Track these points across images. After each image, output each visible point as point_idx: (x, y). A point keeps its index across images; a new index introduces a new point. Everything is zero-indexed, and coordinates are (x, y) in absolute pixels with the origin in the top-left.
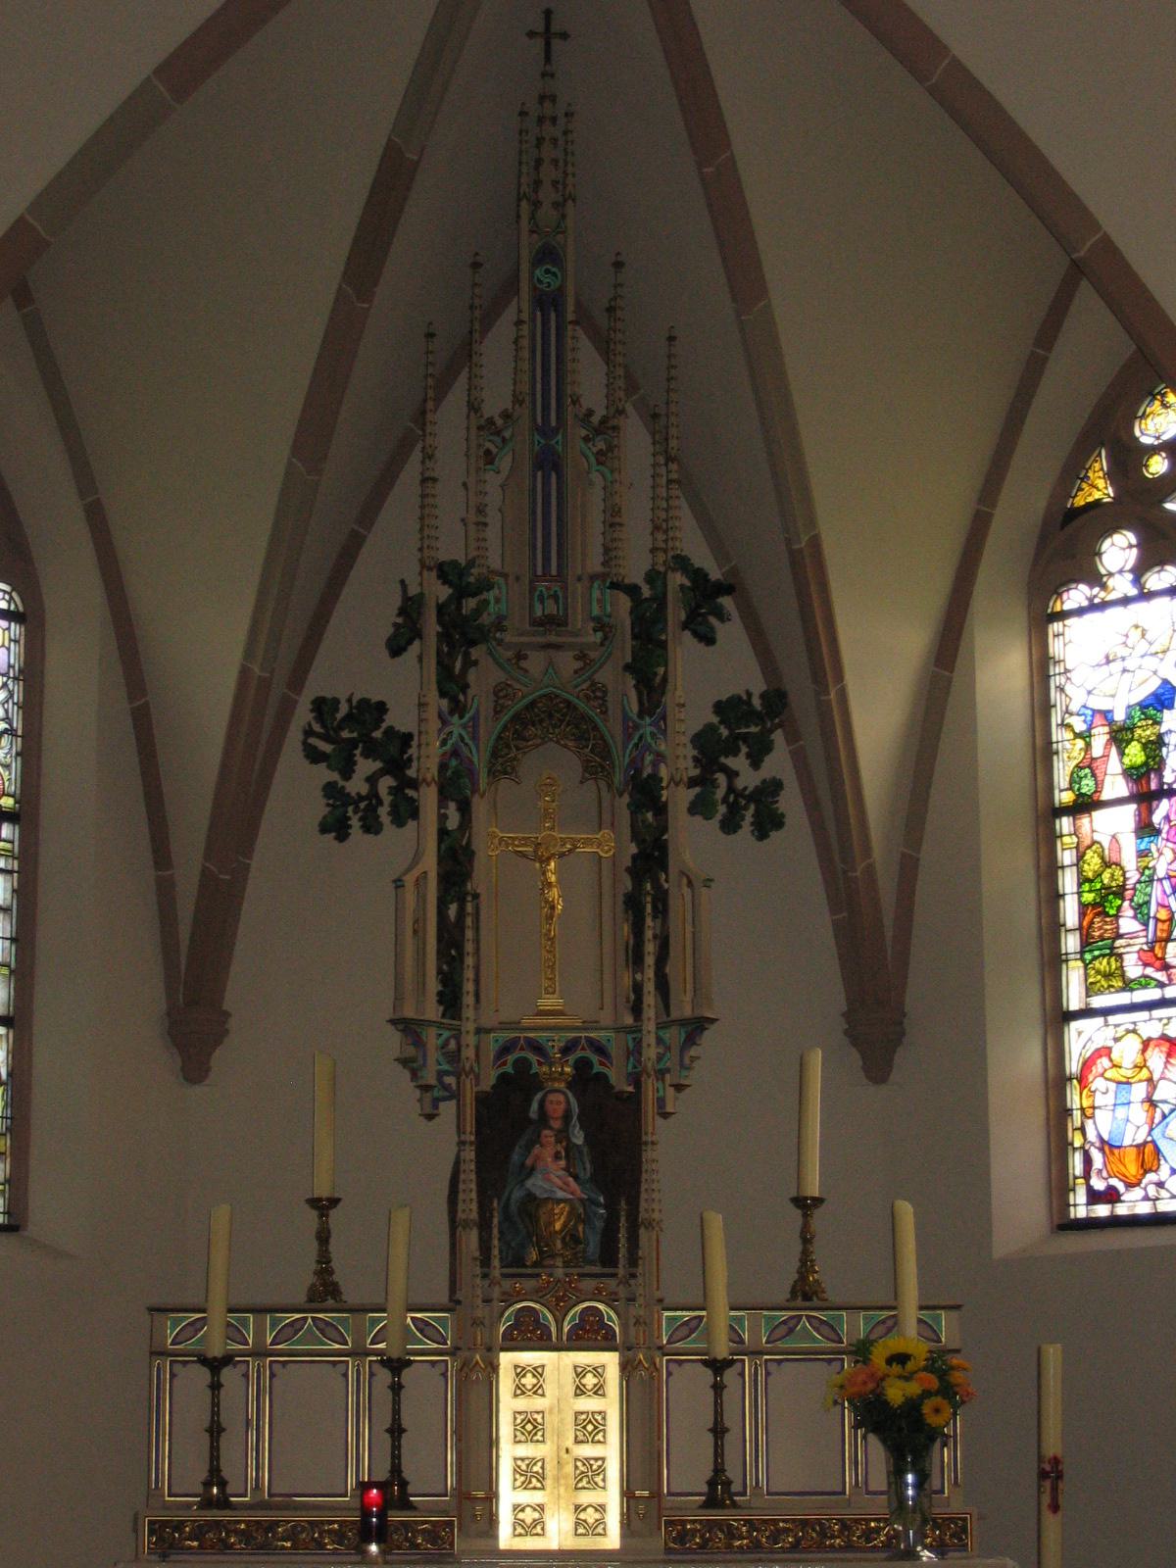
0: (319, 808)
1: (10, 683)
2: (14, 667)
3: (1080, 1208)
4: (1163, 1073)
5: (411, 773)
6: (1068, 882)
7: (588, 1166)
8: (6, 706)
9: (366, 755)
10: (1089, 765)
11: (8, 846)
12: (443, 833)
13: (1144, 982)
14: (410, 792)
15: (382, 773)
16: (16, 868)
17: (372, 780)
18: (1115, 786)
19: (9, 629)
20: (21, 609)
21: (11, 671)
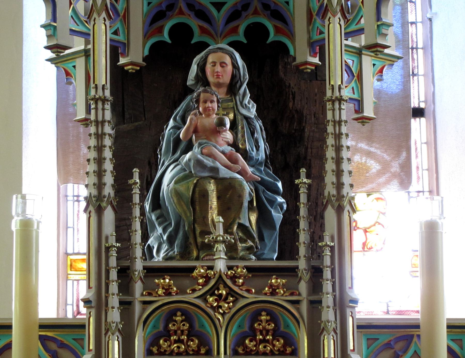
7: (262, 144)
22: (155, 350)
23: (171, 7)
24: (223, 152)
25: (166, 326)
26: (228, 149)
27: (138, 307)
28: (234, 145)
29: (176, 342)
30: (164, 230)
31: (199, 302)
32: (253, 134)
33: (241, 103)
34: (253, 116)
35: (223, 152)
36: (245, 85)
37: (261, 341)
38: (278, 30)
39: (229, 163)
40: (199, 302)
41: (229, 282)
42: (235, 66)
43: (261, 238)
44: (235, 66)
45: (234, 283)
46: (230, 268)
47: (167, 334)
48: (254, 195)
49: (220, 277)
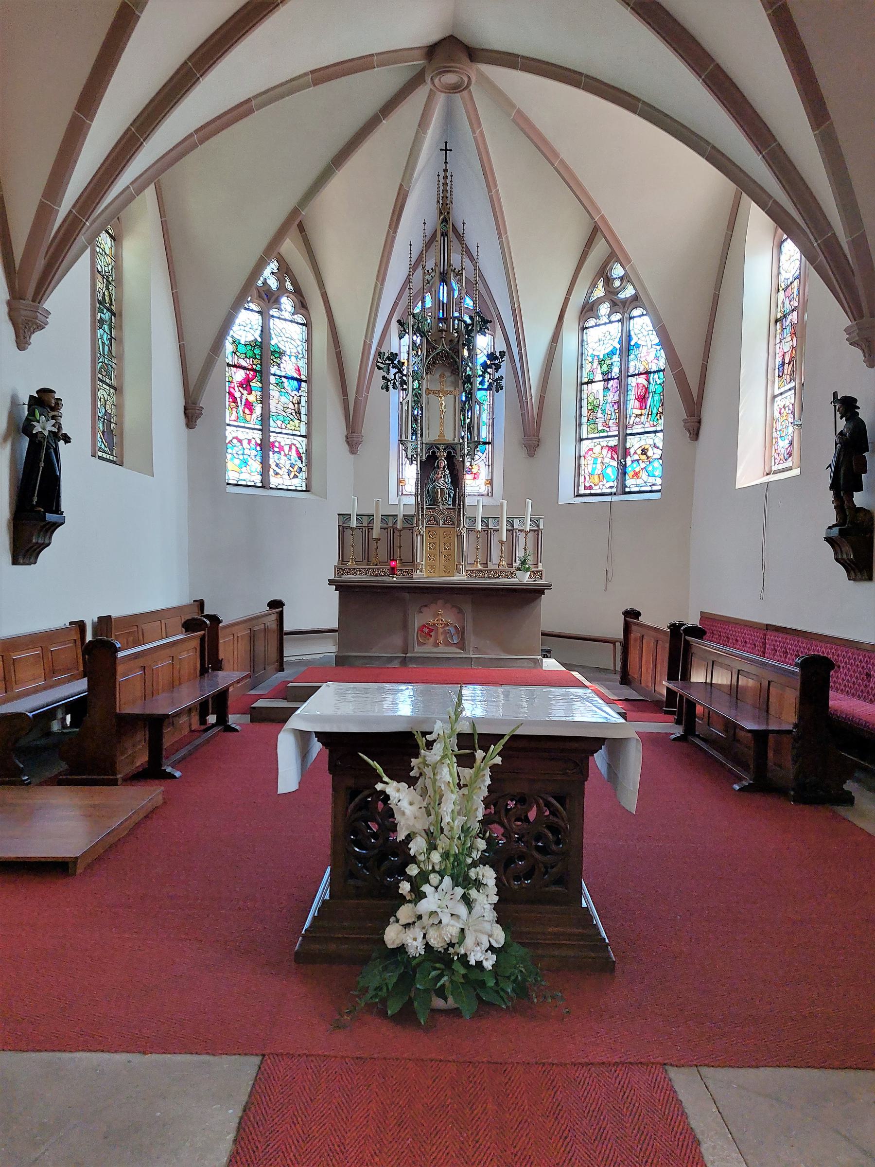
0: (382, 382)
3: (582, 492)
6: (584, 403)
9: (393, 367)
10: (592, 371)
12: (413, 389)
13: (603, 431)
14: (404, 378)
17: (395, 375)
18: (599, 377)
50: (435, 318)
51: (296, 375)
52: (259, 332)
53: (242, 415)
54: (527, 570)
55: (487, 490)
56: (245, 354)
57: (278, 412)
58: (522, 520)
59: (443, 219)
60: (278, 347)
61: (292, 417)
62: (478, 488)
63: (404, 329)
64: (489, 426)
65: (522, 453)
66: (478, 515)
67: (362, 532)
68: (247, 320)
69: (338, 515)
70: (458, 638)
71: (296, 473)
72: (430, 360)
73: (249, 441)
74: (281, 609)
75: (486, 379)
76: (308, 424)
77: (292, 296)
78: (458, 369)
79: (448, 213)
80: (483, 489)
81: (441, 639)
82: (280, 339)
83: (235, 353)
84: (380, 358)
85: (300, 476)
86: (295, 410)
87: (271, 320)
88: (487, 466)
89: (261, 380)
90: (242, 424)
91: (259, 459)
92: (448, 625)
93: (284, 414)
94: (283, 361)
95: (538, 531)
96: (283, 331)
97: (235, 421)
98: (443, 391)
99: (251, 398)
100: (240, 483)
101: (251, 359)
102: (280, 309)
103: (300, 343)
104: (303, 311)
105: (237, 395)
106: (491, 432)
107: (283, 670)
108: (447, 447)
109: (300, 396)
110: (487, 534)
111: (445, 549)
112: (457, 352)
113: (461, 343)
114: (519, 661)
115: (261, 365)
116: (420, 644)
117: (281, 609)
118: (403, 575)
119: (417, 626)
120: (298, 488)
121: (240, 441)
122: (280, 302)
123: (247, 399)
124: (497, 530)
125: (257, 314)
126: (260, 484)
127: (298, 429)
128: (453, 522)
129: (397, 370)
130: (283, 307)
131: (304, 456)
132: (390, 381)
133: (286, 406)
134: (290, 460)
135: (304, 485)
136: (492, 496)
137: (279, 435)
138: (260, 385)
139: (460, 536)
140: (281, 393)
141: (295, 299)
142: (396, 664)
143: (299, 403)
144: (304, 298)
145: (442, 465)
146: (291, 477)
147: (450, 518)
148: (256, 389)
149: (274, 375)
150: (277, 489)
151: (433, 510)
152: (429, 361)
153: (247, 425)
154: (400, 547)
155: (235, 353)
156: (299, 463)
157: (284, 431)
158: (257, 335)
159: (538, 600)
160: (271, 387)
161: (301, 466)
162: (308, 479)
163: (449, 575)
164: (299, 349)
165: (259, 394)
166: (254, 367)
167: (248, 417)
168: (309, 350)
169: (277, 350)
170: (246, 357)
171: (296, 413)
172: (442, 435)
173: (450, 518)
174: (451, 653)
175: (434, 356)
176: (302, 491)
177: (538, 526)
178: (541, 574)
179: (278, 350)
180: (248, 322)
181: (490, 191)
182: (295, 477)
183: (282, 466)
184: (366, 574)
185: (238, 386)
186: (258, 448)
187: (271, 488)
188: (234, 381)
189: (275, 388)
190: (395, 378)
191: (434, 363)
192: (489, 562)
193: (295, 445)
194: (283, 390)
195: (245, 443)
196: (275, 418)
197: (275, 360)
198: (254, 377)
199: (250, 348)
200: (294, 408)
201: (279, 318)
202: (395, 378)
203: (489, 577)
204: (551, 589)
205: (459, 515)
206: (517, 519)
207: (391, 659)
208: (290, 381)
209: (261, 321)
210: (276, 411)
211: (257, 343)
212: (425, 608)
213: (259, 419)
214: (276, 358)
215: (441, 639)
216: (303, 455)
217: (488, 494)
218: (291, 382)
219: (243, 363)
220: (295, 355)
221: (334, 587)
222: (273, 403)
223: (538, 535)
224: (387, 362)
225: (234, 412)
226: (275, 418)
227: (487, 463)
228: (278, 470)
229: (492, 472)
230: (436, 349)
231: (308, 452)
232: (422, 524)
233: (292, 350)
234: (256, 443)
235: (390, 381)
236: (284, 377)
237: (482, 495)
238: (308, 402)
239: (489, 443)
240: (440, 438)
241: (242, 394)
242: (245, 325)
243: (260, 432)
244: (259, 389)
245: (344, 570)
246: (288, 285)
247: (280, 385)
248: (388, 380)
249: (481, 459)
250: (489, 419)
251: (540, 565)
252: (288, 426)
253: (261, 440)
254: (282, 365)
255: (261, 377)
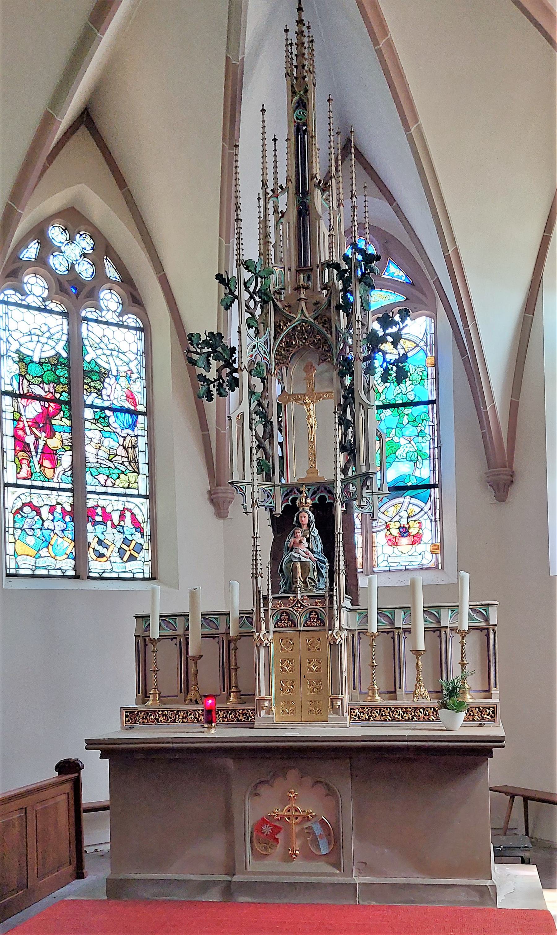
1: (139, 357)
2: (140, 351)
4: (48, 549)
5: (236, 366)
7: (319, 545)
8: (137, 367)
11: (143, 426)
12: (252, 393)
14: (235, 375)
15: (224, 367)
16: (146, 435)
19: (136, 334)
20: (142, 326)
21: (139, 352)
22: (276, 626)
23: (291, 491)
24: (303, 551)
25: (280, 618)
26: (305, 550)
27: (270, 611)
28: (308, 548)
29: (284, 623)
30: (284, 580)
31: (291, 609)
32: (316, 542)
33: (312, 530)
34: (316, 535)
35: (303, 551)
36: (314, 523)
37: (313, 622)
38: (330, 498)
39: (306, 555)
40: (291, 609)
41: (301, 601)
42: (309, 517)
43: (319, 581)
44: (309, 517)
45: (303, 602)
46: (302, 596)
47: (281, 620)
48: (316, 566)
49: (298, 600)
50: (290, 270)
51: (127, 405)
52: (62, 344)
53: (38, 470)
54: (459, 706)
55: (434, 560)
56: (41, 376)
57: (100, 461)
58: (454, 608)
59: (298, 102)
60: (97, 364)
61: (123, 468)
62: (420, 558)
63: (230, 290)
64: (434, 459)
65: (489, 496)
66: (371, 605)
67: (218, 643)
68: (43, 326)
69: (136, 617)
70: (329, 844)
71: (132, 552)
72: (282, 340)
73: (52, 509)
74: (77, 775)
75: (377, 363)
76: (151, 477)
77: (117, 287)
78: (330, 350)
79: (306, 91)
80: (429, 559)
81: (297, 845)
82: (99, 352)
83: (24, 377)
84: (192, 344)
85: (140, 556)
86: (128, 458)
87: (84, 326)
88: (433, 523)
89: (70, 415)
90: (40, 484)
91: (69, 534)
92: (308, 819)
93: (110, 464)
94: (106, 385)
95: (487, 629)
96: (105, 340)
97: (26, 478)
98: (310, 393)
99: (54, 443)
100: (38, 572)
101: (52, 385)
102: (98, 308)
103: (132, 357)
104: (136, 309)
105: (30, 439)
106: (437, 468)
107: (80, 875)
108: (318, 489)
109: (137, 436)
110: (393, 638)
111: (311, 670)
112: (327, 322)
113: (333, 304)
114: (449, 890)
115: (69, 393)
116: (259, 856)
117: (77, 775)
118: (238, 720)
119: (250, 824)
120: (137, 576)
121: (37, 510)
122: (98, 297)
123: (46, 444)
124: (408, 631)
125: (59, 317)
126: (72, 573)
127: (135, 485)
128: (322, 622)
129: (222, 363)
130: (102, 304)
131: (146, 527)
132: (212, 382)
133: (112, 452)
134: (123, 533)
135: (147, 569)
136: (443, 568)
137: (101, 497)
138: (68, 423)
139: (334, 645)
140: (104, 433)
141: (121, 290)
142: (214, 896)
143: (134, 447)
144: (136, 289)
145: (305, 521)
146: (125, 559)
147: (317, 614)
148: (61, 429)
149: (92, 406)
150: (101, 578)
151: (286, 601)
152: (280, 343)
153: (46, 484)
154: (236, 670)
155: (24, 377)
156: (137, 538)
157: (110, 490)
158: (60, 348)
159: (480, 769)
160: (88, 425)
161: (141, 541)
162: (154, 561)
163: (319, 717)
164: (133, 366)
165: (66, 436)
166: (57, 395)
167: (49, 473)
168: (149, 367)
169: (95, 369)
170: (43, 382)
171: (130, 462)
172: (312, 469)
173: (317, 614)
174: (314, 874)
175: (288, 333)
176: (144, 579)
177: (487, 620)
178: (493, 712)
179: (97, 369)
180: (44, 329)
181: (376, 42)
182: (132, 558)
183: (110, 544)
184: (174, 721)
185: (29, 426)
186: (68, 518)
187: (90, 578)
188: (24, 418)
189: (94, 426)
190: (220, 377)
191: (289, 345)
192: (398, 689)
193: (130, 510)
194: (107, 429)
195: (45, 511)
196: (95, 472)
197: (92, 384)
198: (58, 410)
199: (49, 368)
200: (126, 455)
201: (97, 321)
202: (220, 377)
203: (394, 719)
204: (503, 747)
205: (331, 608)
206: (447, 609)
207: (205, 886)
208: (119, 414)
209: (66, 327)
210: (95, 460)
211: (62, 360)
212: (266, 786)
213: (69, 473)
214: (93, 381)
215: (297, 845)
216: (144, 525)
217: (437, 565)
218: (121, 415)
219: (38, 391)
220: (124, 374)
221: (99, 752)
222: (90, 450)
223: (488, 635)
224: (205, 350)
225: (25, 466)
226: (95, 472)
227: (433, 518)
228: (102, 550)
229: (442, 531)
230: (290, 321)
231: (152, 519)
232: (267, 627)
233: (120, 369)
234: (63, 509)
235: (212, 382)
236: (110, 409)
237: (427, 569)
238: (150, 445)
239: (434, 486)
240: (310, 475)
241: (37, 438)
242: (40, 334)
243: (70, 494)
244: (68, 429)
245: (137, 715)
246: (111, 272)
247: (102, 420)
248: (208, 382)
249: (423, 512)
250: (434, 448)
251: (494, 691)
252: (118, 482)
253: (71, 506)
254: (104, 392)
255: (70, 410)
